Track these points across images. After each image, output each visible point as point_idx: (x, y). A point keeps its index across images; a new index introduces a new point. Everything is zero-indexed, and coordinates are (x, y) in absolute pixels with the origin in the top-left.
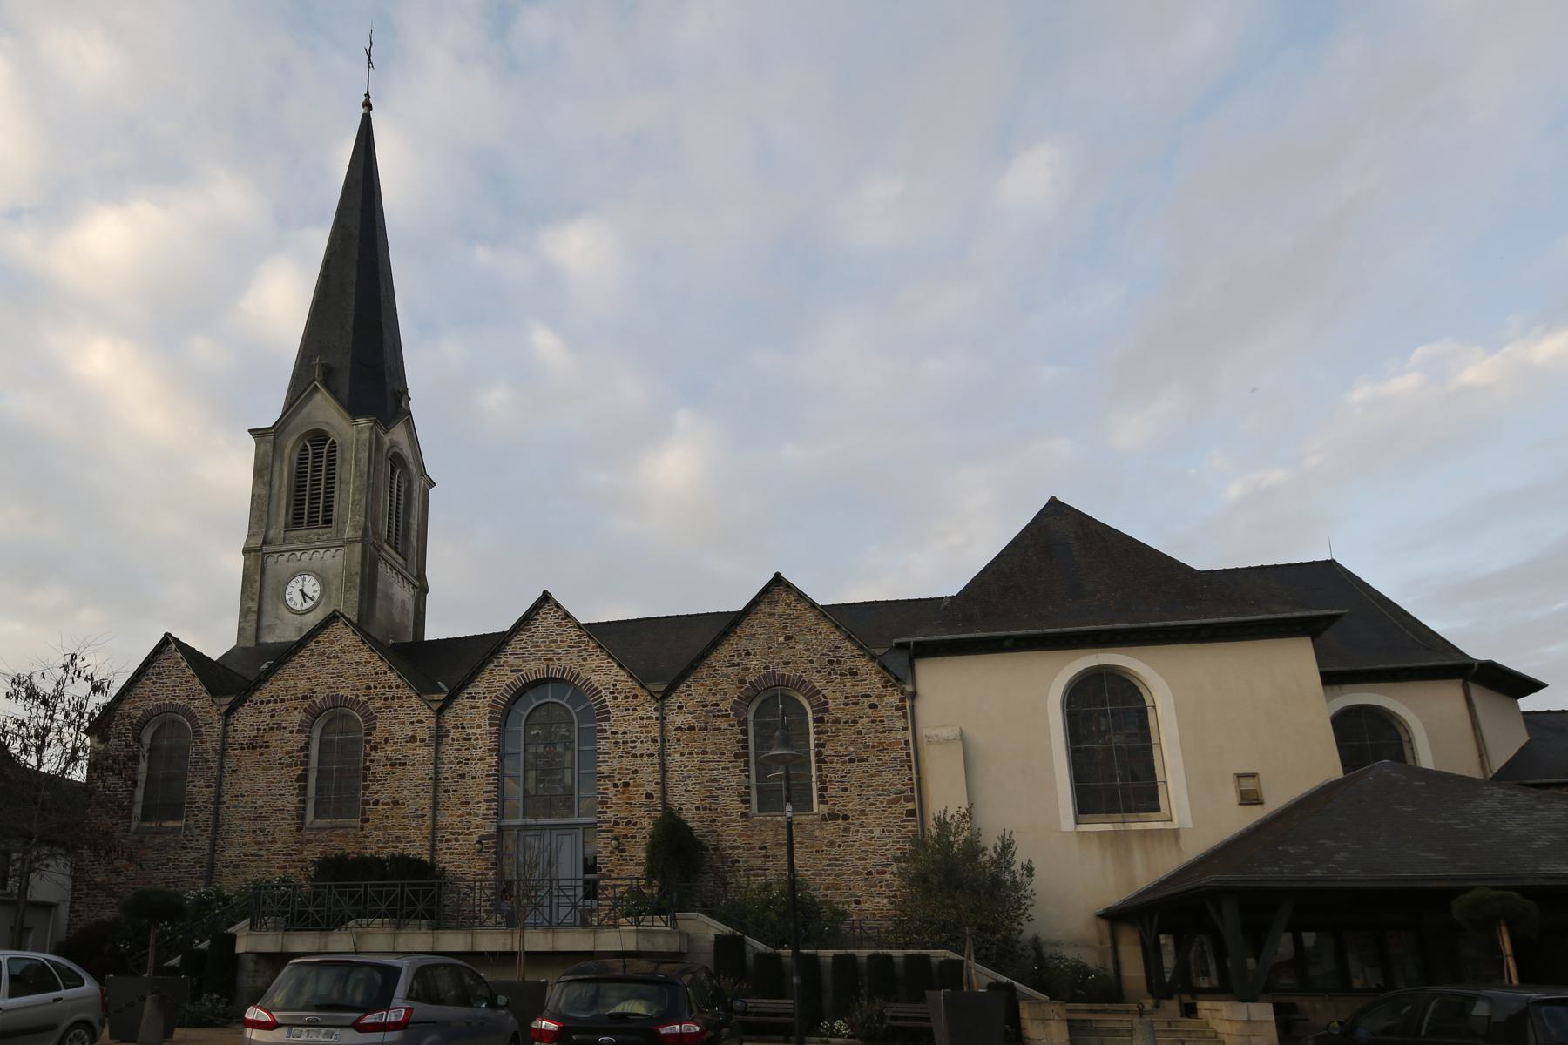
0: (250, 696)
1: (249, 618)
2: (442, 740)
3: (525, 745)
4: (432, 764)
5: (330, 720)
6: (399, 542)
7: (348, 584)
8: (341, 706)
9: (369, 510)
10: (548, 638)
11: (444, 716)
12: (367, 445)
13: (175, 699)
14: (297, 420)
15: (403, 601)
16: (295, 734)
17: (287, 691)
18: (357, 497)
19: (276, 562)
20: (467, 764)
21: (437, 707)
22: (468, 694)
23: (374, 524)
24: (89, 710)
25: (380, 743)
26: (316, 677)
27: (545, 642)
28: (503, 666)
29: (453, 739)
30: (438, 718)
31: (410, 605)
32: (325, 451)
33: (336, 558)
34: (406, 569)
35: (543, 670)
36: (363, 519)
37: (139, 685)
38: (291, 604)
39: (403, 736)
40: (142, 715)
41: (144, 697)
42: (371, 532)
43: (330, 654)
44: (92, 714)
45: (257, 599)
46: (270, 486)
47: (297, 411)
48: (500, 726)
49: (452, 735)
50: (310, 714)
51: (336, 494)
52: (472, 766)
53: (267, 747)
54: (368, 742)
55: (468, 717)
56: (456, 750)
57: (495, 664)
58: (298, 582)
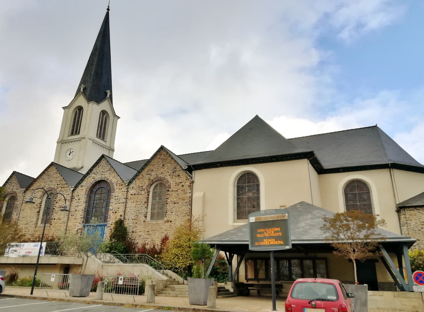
20: (78, 207)
49: (75, 198)
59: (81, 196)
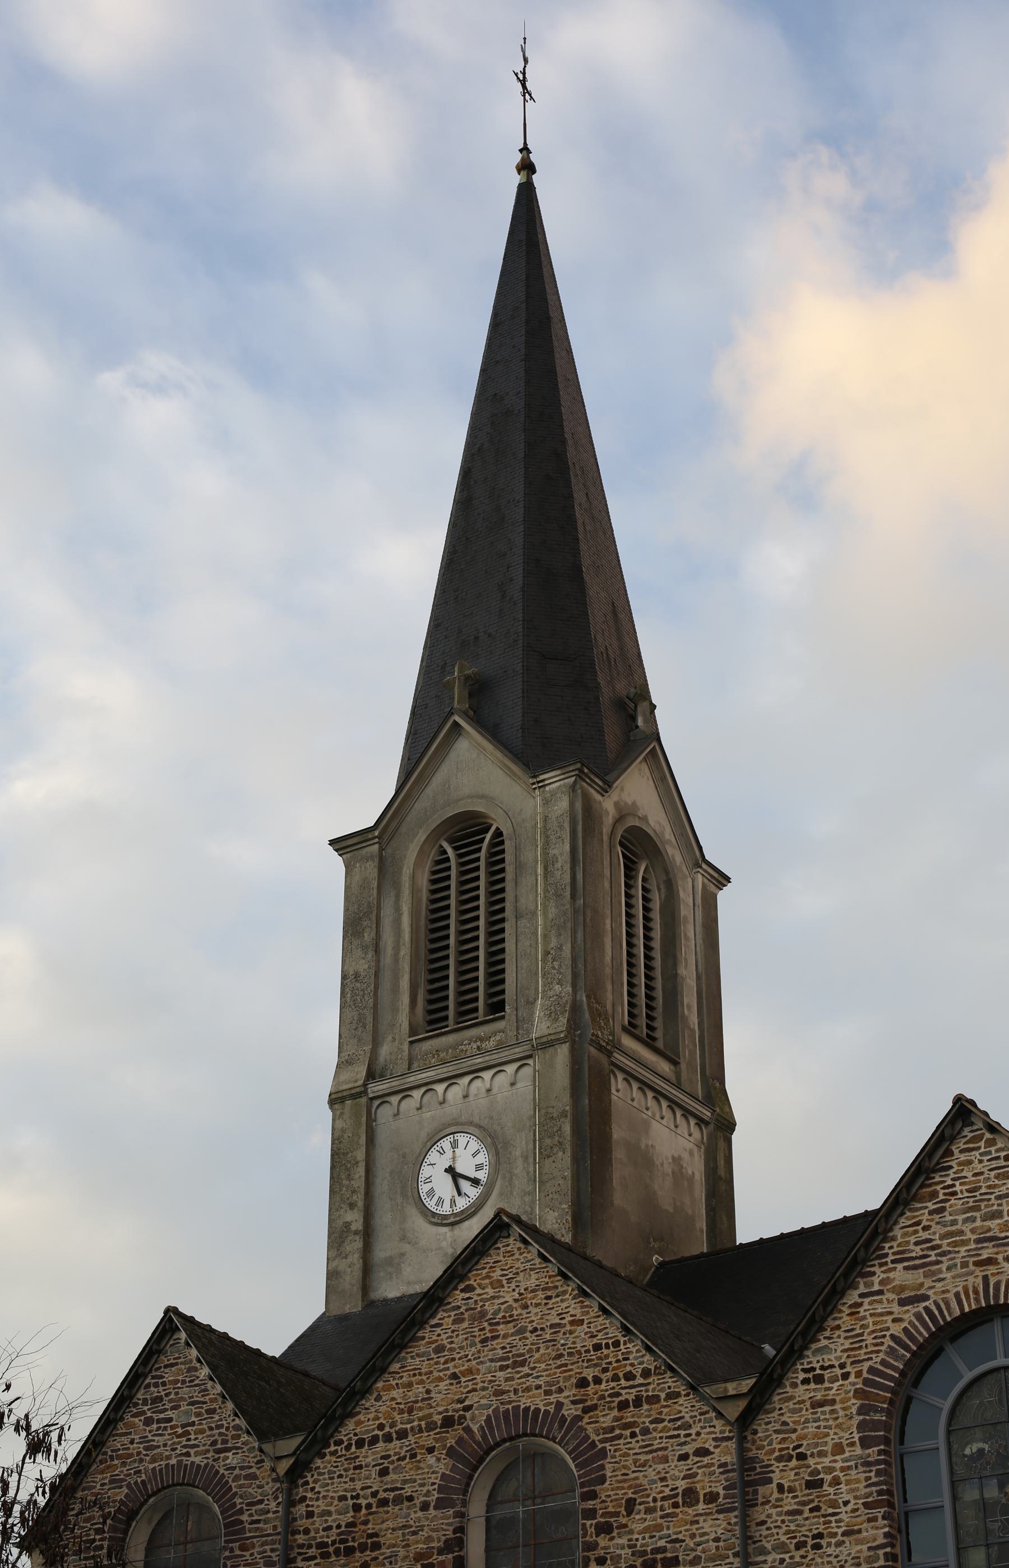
0: (336, 1430)
1: (348, 1248)
2: (756, 1492)
3: (953, 1484)
4: (736, 1555)
5: (510, 1464)
6: (658, 1024)
7: (548, 1141)
8: (525, 1435)
9: (581, 966)
10: (977, 1208)
11: (755, 1432)
12: (567, 826)
13: (188, 1454)
14: (422, 803)
15: (677, 1160)
16: (432, 1512)
17: (410, 1411)
18: (554, 943)
19: (397, 1114)
20: (817, 1547)
21: (737, 1414)
22: (805, 1371)
23: (594, 994)
24: (23, 1497)
25: (617, 1514)
26: (470, 1371)
27: (973, 1220)
28: (880, 1292)
29: (780, 1488)
30: (742, 1440)
31: (696, 1167)
32: (483, 854)
33: (519, 1085)
34: (678, 1086)
35: (976, 1292)
36: (569, 989)
37: (121, 1428)
38: (431, 1204)
39: (667, 1492)
40: (127, 1496)
41: (131, 1455)
42: (587, 1015)
43: (496, 1313)
44: (32, 1502)
45: (361, 1204)
46: (377, 951)
47: (424, 780)
48: (887, 1441)
49: (776, 1477)
50: (461, 1458)
51: (509, 945)
52: (830, 1551)
53: (376, 1546)
54: (591, 1514)
55: (811, 1428)
56: (790, 1513)
57: (862, 1289)
58: (442, 1152)
59: (822, 1454)
